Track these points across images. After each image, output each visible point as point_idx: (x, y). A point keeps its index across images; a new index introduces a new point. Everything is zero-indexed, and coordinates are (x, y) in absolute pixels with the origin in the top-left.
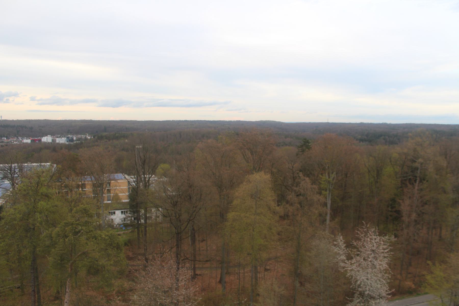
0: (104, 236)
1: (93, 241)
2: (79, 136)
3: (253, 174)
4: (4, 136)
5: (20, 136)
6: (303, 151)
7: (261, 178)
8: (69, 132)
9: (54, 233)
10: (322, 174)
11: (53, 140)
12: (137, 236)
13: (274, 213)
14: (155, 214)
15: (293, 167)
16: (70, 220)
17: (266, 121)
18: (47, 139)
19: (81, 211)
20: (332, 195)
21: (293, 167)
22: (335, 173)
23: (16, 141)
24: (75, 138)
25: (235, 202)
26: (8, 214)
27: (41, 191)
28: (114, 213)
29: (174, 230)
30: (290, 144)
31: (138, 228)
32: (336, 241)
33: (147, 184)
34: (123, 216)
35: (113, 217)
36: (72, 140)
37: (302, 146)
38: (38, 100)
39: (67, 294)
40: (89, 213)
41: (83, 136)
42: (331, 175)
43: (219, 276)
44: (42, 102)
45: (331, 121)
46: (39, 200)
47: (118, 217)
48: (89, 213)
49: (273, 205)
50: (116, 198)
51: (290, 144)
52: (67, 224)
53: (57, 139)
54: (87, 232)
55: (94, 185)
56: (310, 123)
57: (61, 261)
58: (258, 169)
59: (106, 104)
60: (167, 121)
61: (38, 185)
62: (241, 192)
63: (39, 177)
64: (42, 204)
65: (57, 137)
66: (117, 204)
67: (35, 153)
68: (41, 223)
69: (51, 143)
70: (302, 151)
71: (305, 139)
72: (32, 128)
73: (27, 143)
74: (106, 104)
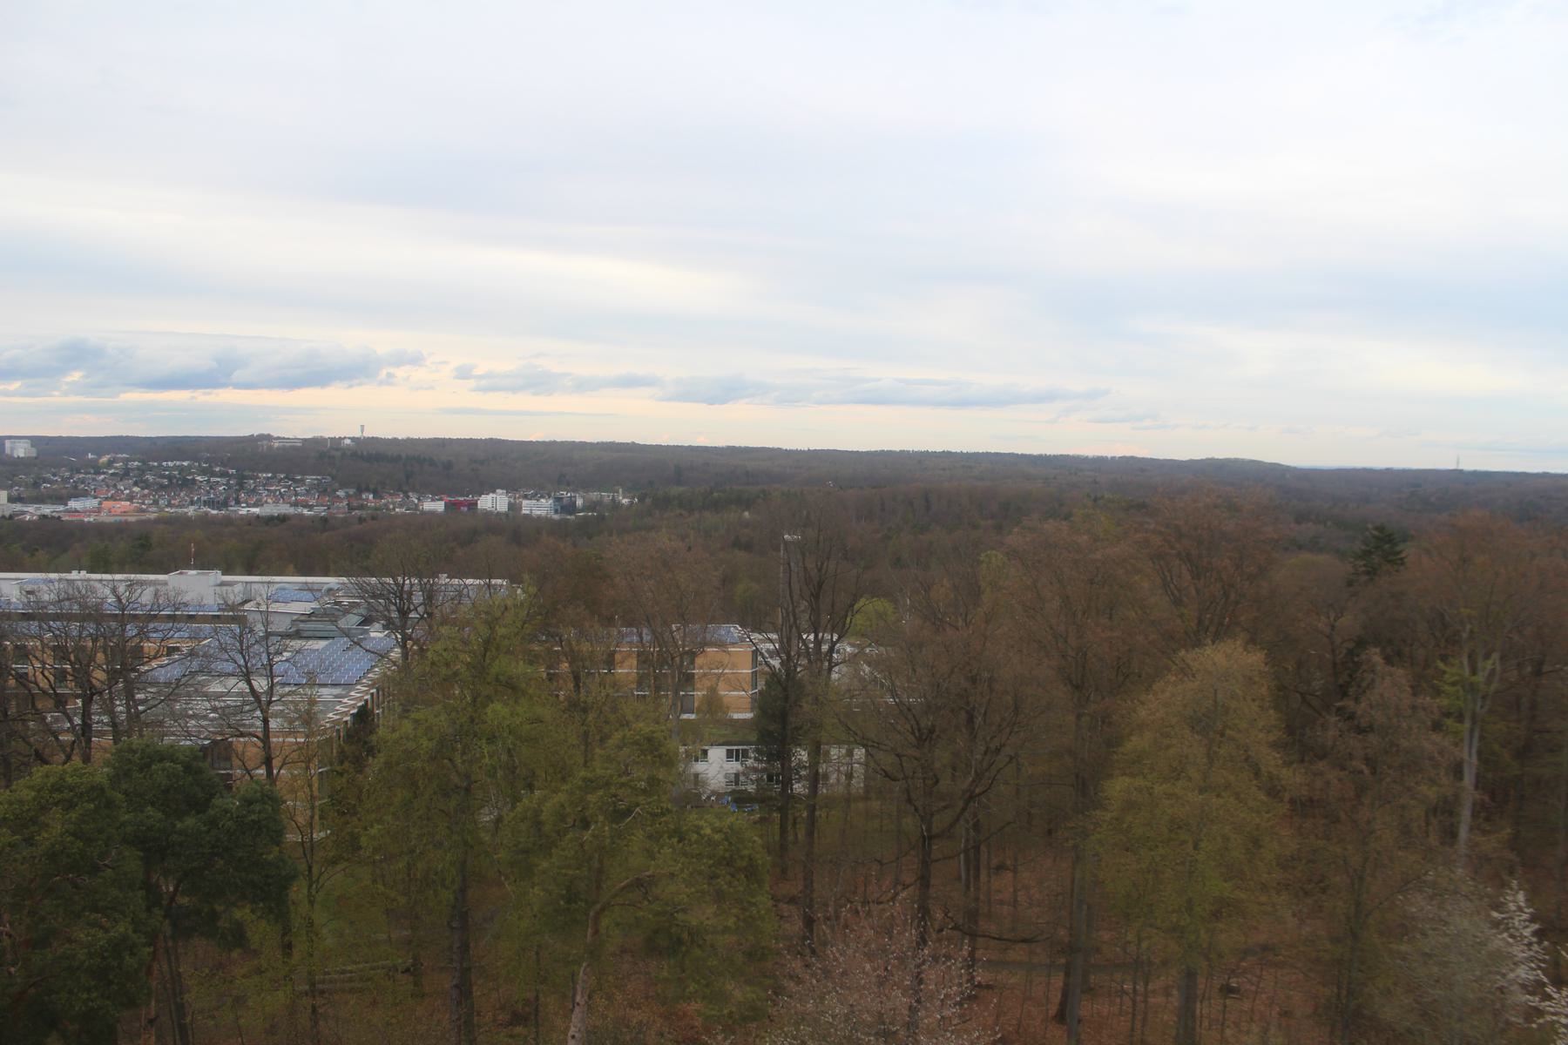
0: (708, 831)
1: (671, 846)
2: (594, 495)
3: (1198, 644)
4: (368, 490)
5: (413, 490)
6: (1372, 572)
7: (1229, 662)
8: (562, 481)
9: (548, 807)
10: (1444, 658)
11: (510, 504)
12: (777, 838)
13: (1273, 792)
14: (845, 764)
15: (1333, 627)
16: (599, 772)
17: (1228, 460)
18: (494, 502)
19: (636, 743)
20: (1482, 738)
21: (1333, 627)
22: (1496, 656)
23: (401, 506)
24: (579, 502)
25: (1135, 743)
26: (396, 735)
27: (494, 670)
28: (705, 752)
29: (910, 822)
30: (1314, 545)
31: (783, 810)
32: (1498, 907)
33: (822, 660)
34: (735, 766)
35: (700, 767)
36: (570, 508)
37: (1366, 554)
38: (480, 377)
39: (577, 1009)
40: (663, 750)
41: (606, 497)
42: (1480, 665)
43: (1056, 998)
44: (492, 384)
45: (1468, 465)
46: (489, 699)
47: (716, 767)
48: (663, 750)
49: (1271, 760)
50: (713, 704)
51: (1314, 545)
52: (590, 785)
53: (525, 502)
54: (653, 815)
55: (643, 658)
56: (1388, 471)
57: (569, 901)
58: (1212, 629)
59: (688, 393)
60: (1365, 470)
61: (486, 650)
62: (1160, 704)
63: (491, 624)
64: (497, 711)
65: (526, 497)
66: (714, 725)
67: (464, 543)
68: (492, 773)
69: (506, 514)
70: (1368, 573)
71: (1380, 529)
72: (448, 466)
73: (433, 513)
74: (688, 393)
